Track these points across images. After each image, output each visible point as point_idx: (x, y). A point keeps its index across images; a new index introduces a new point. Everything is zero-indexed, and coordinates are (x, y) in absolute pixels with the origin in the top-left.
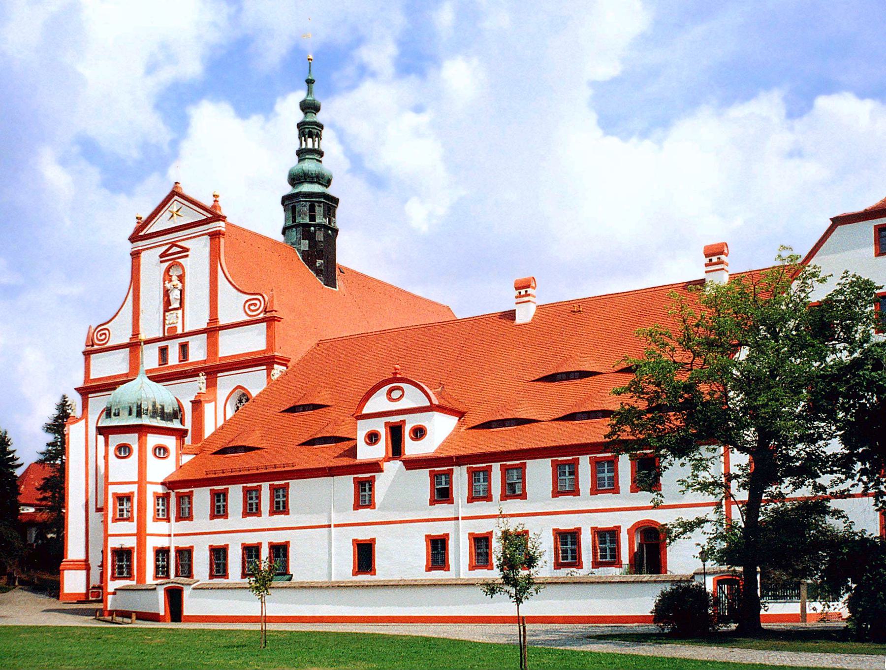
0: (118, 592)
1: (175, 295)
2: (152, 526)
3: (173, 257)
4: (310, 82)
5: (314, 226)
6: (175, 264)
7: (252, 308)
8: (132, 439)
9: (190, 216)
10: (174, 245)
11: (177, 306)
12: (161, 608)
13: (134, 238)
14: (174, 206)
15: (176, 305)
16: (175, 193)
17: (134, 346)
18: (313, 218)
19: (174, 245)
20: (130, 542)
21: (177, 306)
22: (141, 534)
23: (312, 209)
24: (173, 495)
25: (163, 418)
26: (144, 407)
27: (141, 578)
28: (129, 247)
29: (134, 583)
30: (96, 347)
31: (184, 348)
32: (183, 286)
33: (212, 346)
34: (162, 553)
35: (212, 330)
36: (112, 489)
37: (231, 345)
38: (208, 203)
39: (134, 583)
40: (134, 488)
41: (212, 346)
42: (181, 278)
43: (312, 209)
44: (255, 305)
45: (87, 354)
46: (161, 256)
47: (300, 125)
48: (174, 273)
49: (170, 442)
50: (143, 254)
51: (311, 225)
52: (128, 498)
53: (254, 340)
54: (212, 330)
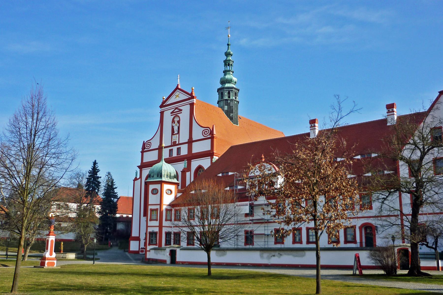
0: (151, 251)
1: (176, 128)
2: (165, 223)
3: (176, 113)
4: (228, 45)
5: (230, 100)
6: (176, 116)
7: (206, 133)
8: (158, 186)
9: (183, 97)
10: (176, 108)
11: (177, 133)
12: (168, 261)
13: (161, 106)
14: (177, 93)
15: (176, 132)
16: (177, 88)
17: (160, 149)
18: (229, 97)
19: (176, 108)
20: (157, 230)
21: (177, 133)
22: (161, 226)
23: (229, 93)
24: (173, 212)
25: (170, 178)
26: (163, 173)
27: (160, 245)
28: (159, 110)
29: (157, 247)
30: (146, 150)
31: (179, 149)
32: (179, 125)
33: (190, 149)
34: (168, 234)
35: (190, 142)
36: (150, 207)
37: (197, 148)
38: (190, 92)
39: (157, 247)
40: (158, 207)
41: (190, 149)
42: (179, 122)
43: (229, 93)
44: (207, 132)
45: (142, 152)
46: (171, 113)
47: (225, 61)
48: (176, 119)
49: (173, 187)
50: (165, 113)
51: (228, 100)
52: (156, 210)
53: (204, 146)
54: (190, 142)
